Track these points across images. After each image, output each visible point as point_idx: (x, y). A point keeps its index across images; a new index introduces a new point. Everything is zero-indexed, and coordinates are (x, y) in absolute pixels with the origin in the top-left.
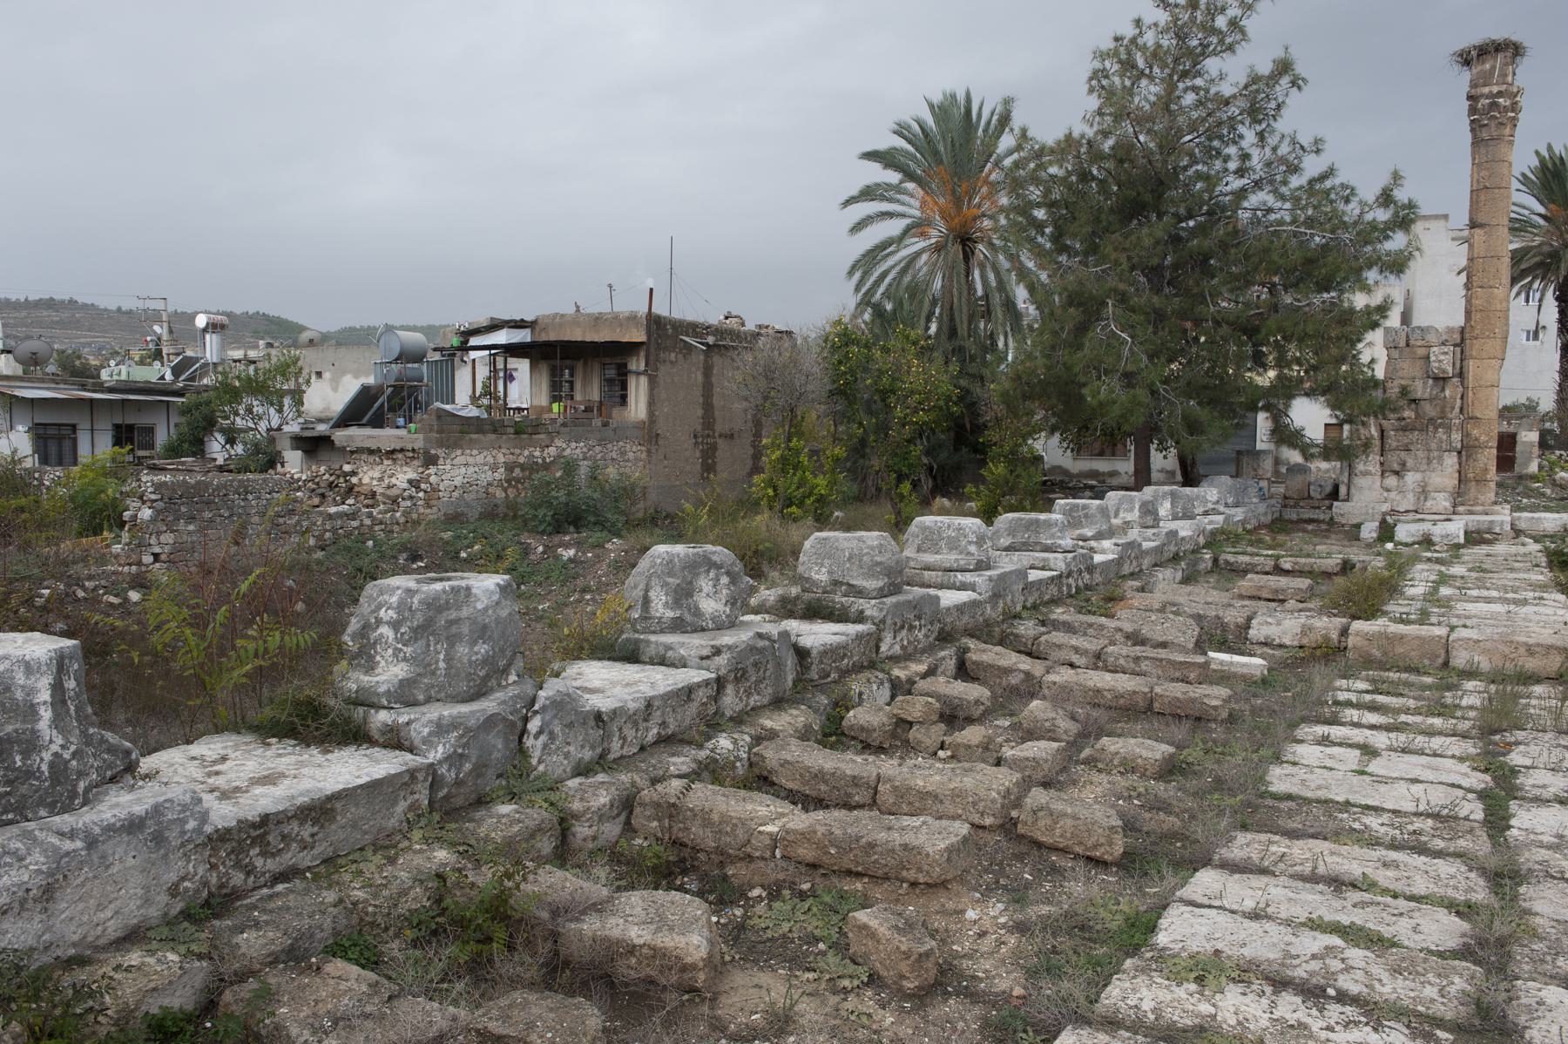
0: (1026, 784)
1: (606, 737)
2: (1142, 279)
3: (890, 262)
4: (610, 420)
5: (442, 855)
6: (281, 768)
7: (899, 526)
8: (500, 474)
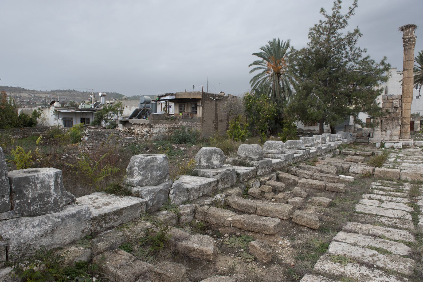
0: (294, 209)
1: (190, 195)
2: (322, 83)
3: (260, 79)
4: (192, 118)
5: (148, 224)
6: (110, 201)
7: (262, 143)
8: (167, 130)
